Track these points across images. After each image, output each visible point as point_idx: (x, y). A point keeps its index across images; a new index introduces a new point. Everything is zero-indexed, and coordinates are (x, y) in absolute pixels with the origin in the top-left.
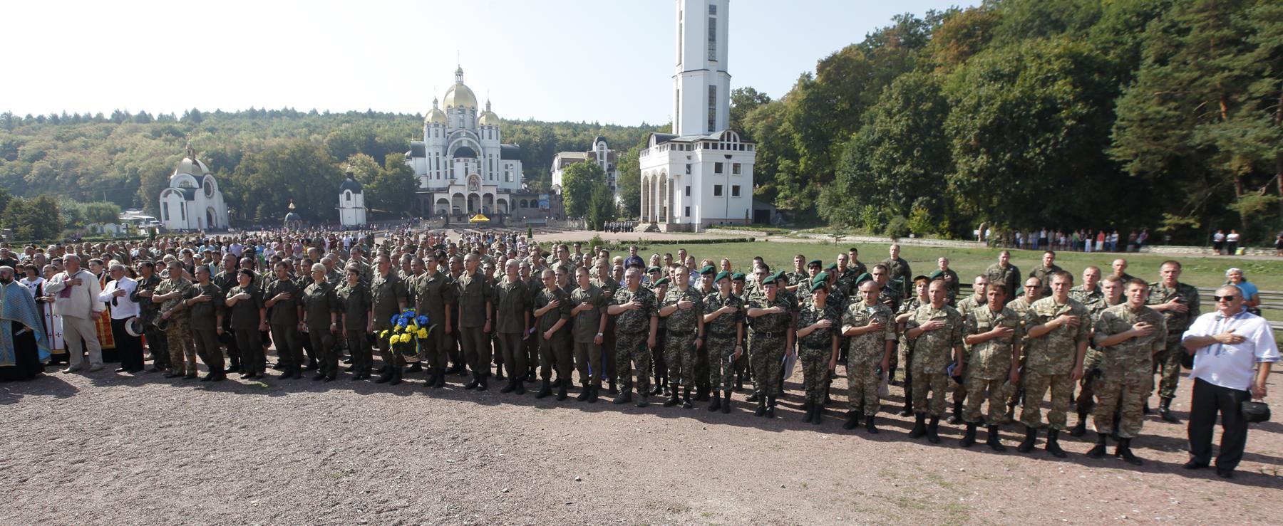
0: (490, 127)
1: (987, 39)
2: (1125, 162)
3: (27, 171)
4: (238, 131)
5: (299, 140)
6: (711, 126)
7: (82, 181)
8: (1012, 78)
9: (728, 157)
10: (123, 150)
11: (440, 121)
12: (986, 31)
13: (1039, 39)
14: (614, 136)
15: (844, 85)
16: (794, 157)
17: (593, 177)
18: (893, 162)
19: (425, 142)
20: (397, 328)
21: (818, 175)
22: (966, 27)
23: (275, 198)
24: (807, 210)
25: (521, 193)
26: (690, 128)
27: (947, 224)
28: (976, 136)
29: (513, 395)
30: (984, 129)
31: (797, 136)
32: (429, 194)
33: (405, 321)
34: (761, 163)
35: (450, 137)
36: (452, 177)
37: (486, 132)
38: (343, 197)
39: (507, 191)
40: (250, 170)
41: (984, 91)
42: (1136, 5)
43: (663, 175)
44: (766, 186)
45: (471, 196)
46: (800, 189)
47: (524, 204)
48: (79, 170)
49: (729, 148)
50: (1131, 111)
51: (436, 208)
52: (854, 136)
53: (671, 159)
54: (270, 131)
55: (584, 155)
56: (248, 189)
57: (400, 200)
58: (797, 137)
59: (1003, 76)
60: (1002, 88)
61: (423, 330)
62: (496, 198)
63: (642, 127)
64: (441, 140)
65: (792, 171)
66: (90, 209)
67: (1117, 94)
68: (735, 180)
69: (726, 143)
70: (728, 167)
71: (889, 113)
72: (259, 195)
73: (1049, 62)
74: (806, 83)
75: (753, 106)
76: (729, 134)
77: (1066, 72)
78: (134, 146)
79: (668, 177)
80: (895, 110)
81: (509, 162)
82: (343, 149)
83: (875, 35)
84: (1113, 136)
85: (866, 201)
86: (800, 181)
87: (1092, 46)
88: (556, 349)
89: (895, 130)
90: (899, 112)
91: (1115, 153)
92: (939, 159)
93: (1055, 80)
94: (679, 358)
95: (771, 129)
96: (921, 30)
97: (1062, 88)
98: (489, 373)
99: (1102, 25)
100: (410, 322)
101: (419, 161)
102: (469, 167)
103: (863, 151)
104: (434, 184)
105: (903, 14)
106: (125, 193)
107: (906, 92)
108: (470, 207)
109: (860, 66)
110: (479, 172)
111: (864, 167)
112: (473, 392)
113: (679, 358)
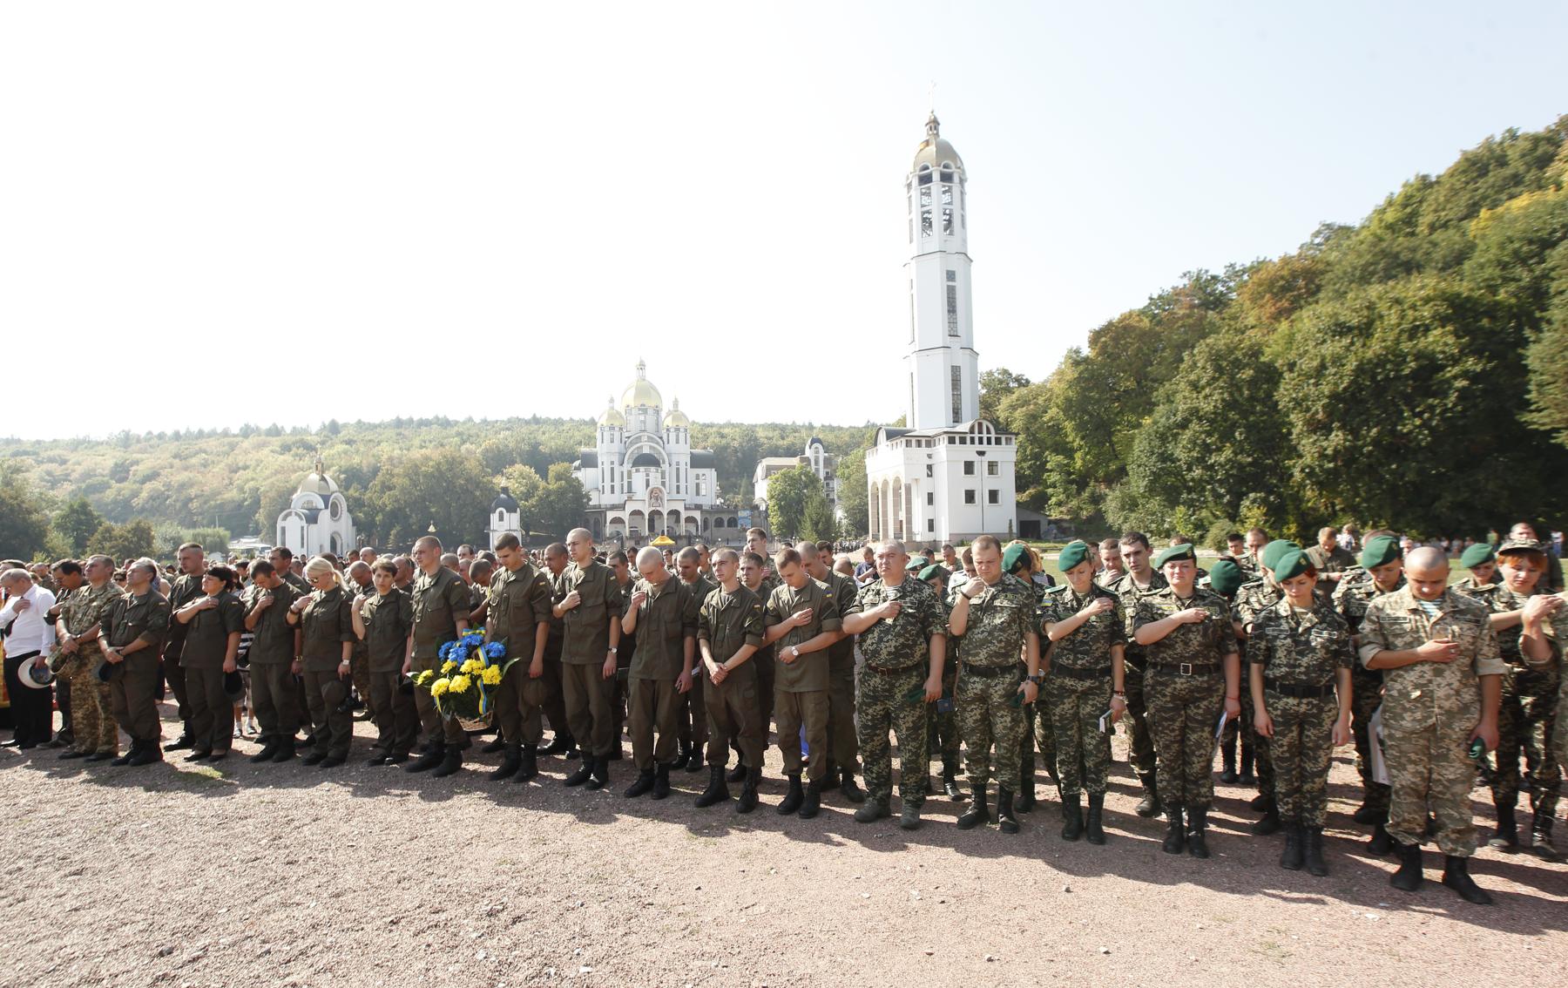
0: (677, 429)
1: (1314, 292)
2: (1557, 430)
3: (135, 494)
4: (379, 443)
5: (448, 450)
6: (957, 416)
7: (194, 505)
8: (1365, 330)
9: (981, 453)
10: (246, 468)
11: (617, 424)
12: (1312, 281)
13: (1391, 283)
14: (830, 438)
15: (1124, 366)
16: (1069, 452)
17: (806, 487)
18: (1207, 449)
19: (598, 449)
20: (447, 667)
21: (1101, 473)
22: (1282, 278)
23: (413, 519)
24: (1089, 520)
25: (715, 510)
26: (934, 420)
27: (1293, 528)
28: (1324, 406)
29: (647, 802)
30: (1334, 396)
31: (1069, 426)
32: (601, 512)
33: (462, 651)
34: (1024, 460)
35: (628, 442)
36: (630, 491)
37: (673, 436)
38: (494, 517)
39: (698, 507)
40: (386, 487)
41: (1329, 349)
42: (1525, 232)
43: (897, 480)
44: (1032, 491)
45: (652, 514)
46: (1079, 493)
47: (719, 523)
48: (193, 492)
49: (981, 442)
50: (1552, 361)
51: (609, 530)
52: (1147, 421)
53: (908, 462)
54: (417, 442)
55: (795, 461)
56: (382, 509)
57: (562, 512)
58: (1069, 426)
59: (1350, 329)
60: (1352, 344)
61: (495, 669)
62: (684, 515)
63: (866, 427)
64: (617, 447)
65: (1066, 471)
66: (195, 537)
67: (1525, 342)
68: (992, 483)
69: (976, 436)
70: (981, 466)
71: (1195, 386)
72: (395, 516)
73: (1414, 307)
74: (1077, 361)
75: (1009, 391)
76: (980, 425)
77: (1443, 320)
78: (259, 462)
79: (903, 482)
80: (1203, 382)
81: (700, 471)
82: (499, 460)
83: (1160, 297)
84: (1533, 396)
85: (1173, 502)
86: (1080, 482)
87: (1472, 285)
88: (736, 703)
89: (1207, 407)
90: (1208, 384)
91: (1536, 420)
92: (1271, 439)
93: (1427, 329)
94: (986, 722)
95: (1033, 417)
96: (1220, 288)
97: (1440, 340)
98: (617, 752)
99: (1478, 257)
100: (471, 653)
101: (589, 470)
102: (651, 478)
103: (1163, 438)
104: (607, 499)
105: (1194, 271)
106: (241, 519)
107: (1216, 358)
108: (652, 528)
109: (1143, 335)
110: (663, 484)
111: (1165, 458)
112: (577, 791)
113: (986, 722)
